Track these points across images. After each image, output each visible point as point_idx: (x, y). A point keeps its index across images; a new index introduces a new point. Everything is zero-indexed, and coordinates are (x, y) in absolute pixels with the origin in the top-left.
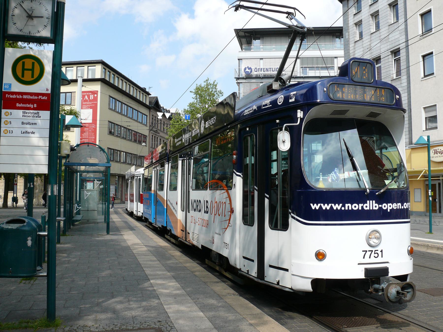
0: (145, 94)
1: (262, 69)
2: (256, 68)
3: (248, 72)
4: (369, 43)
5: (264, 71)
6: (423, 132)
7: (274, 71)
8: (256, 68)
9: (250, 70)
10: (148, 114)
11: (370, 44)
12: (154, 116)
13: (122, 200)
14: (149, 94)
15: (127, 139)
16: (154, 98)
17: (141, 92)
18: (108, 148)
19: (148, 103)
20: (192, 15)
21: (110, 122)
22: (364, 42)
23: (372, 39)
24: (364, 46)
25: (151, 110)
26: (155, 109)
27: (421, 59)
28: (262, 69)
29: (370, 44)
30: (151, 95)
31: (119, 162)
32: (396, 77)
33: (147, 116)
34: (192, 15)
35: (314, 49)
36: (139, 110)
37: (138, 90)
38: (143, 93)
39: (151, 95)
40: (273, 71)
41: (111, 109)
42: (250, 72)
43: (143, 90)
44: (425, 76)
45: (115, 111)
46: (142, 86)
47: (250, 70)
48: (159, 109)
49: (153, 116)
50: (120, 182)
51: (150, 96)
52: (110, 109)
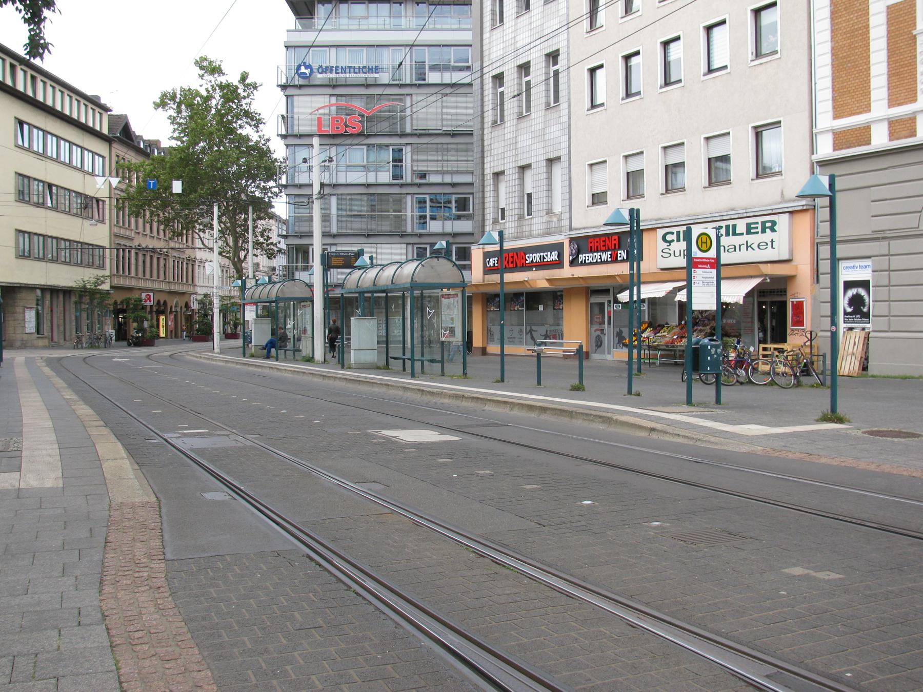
0: (97, 110)
1: (334, 69)
2: (321, 67)
3: (305, 74)
4: (512, 35)
5: (336, 73)
6: (703, 189)
7: (357, 73)
8: (321, 67)
9: (309, 70)
10: (106, 154)
11: (515, 37)
12: (120, 158)
13: (52, 340)
14: (105, 109)
15: (59, 210)
16: (120, 117)
17: (90, 105)
18: (16, 230)
19: (105, 131)
20: (34, 59)
21: (20, 175)
22: (534, 19)
23: (518, 26)
24: (506, 38)
25: (115, 145)
26: (123, 143)
27: (702, 34)
28: (334, 69)
29: (515, 37)
30: (111, 111)
31: (44, 259)
32: (554, 103)
33: (103, 157)
34: (34, 59)
35: (452, 22)
36: (85, 146)
37: (83, 101)
38: (94, 107)
39: (111, 111)
40: (355, 73)
41: (22, 148)
42: (308, 75)
43: (94, 102)
44: (710, 71)
45: (29, 150)
46: (89, 92)
47: (309, 70)
48: (132, 141)
49: (118, 156)
50: (47, 303)
51: (109, 113)
52: (17, 146)
